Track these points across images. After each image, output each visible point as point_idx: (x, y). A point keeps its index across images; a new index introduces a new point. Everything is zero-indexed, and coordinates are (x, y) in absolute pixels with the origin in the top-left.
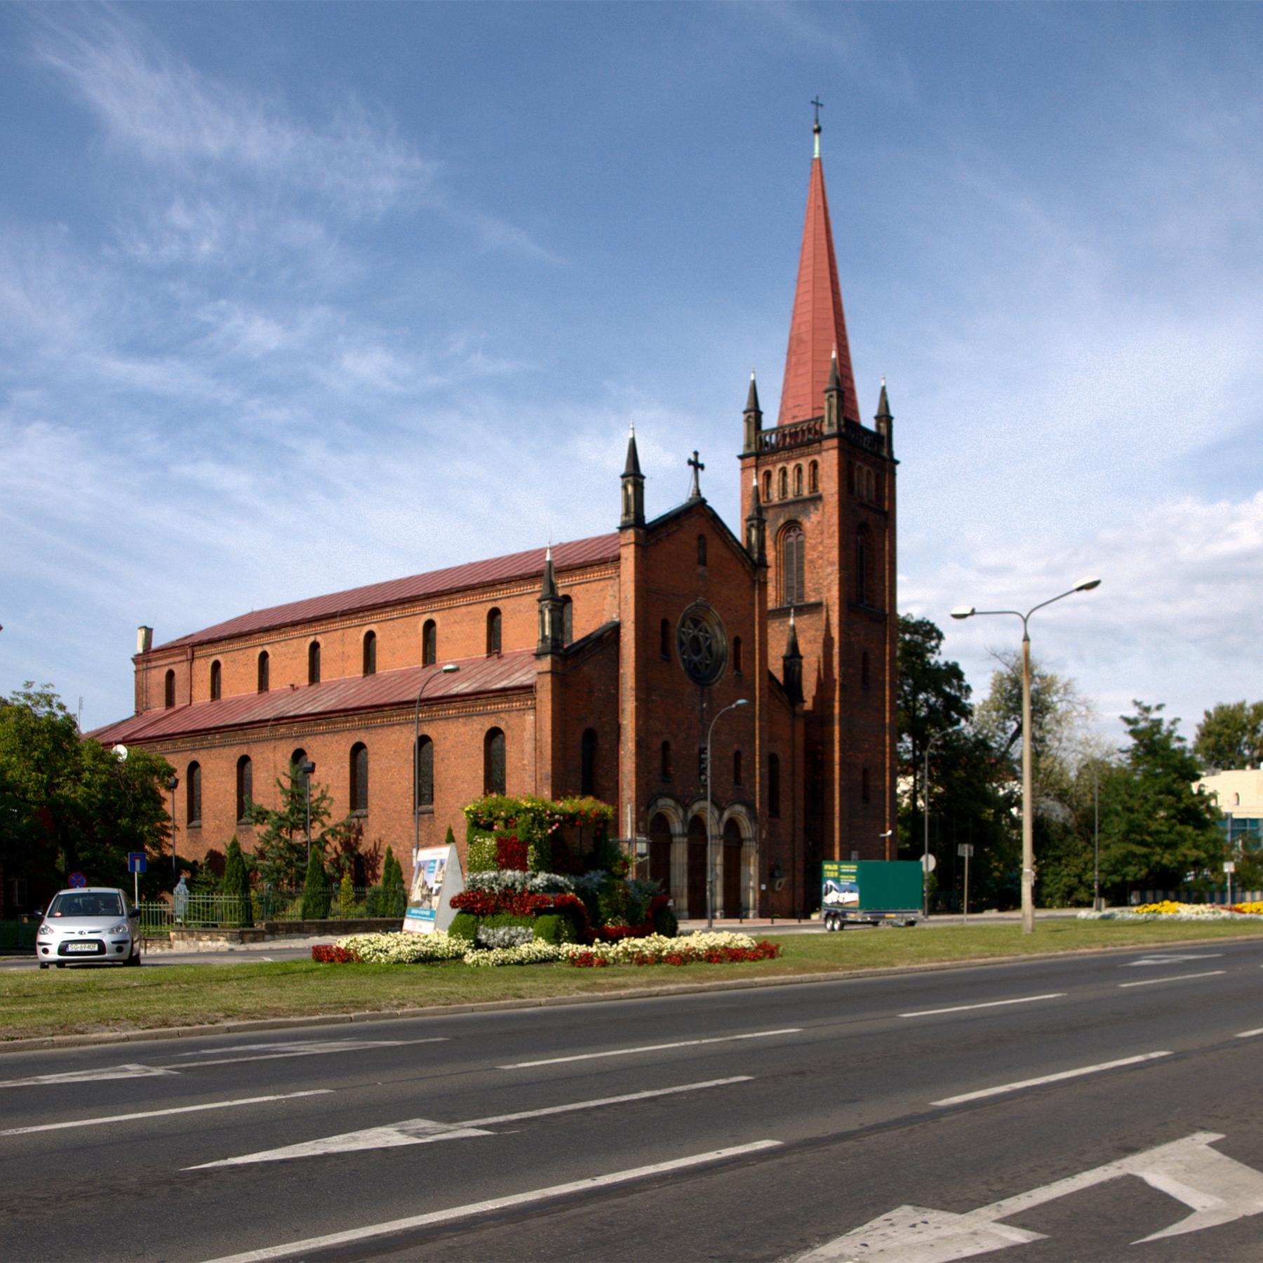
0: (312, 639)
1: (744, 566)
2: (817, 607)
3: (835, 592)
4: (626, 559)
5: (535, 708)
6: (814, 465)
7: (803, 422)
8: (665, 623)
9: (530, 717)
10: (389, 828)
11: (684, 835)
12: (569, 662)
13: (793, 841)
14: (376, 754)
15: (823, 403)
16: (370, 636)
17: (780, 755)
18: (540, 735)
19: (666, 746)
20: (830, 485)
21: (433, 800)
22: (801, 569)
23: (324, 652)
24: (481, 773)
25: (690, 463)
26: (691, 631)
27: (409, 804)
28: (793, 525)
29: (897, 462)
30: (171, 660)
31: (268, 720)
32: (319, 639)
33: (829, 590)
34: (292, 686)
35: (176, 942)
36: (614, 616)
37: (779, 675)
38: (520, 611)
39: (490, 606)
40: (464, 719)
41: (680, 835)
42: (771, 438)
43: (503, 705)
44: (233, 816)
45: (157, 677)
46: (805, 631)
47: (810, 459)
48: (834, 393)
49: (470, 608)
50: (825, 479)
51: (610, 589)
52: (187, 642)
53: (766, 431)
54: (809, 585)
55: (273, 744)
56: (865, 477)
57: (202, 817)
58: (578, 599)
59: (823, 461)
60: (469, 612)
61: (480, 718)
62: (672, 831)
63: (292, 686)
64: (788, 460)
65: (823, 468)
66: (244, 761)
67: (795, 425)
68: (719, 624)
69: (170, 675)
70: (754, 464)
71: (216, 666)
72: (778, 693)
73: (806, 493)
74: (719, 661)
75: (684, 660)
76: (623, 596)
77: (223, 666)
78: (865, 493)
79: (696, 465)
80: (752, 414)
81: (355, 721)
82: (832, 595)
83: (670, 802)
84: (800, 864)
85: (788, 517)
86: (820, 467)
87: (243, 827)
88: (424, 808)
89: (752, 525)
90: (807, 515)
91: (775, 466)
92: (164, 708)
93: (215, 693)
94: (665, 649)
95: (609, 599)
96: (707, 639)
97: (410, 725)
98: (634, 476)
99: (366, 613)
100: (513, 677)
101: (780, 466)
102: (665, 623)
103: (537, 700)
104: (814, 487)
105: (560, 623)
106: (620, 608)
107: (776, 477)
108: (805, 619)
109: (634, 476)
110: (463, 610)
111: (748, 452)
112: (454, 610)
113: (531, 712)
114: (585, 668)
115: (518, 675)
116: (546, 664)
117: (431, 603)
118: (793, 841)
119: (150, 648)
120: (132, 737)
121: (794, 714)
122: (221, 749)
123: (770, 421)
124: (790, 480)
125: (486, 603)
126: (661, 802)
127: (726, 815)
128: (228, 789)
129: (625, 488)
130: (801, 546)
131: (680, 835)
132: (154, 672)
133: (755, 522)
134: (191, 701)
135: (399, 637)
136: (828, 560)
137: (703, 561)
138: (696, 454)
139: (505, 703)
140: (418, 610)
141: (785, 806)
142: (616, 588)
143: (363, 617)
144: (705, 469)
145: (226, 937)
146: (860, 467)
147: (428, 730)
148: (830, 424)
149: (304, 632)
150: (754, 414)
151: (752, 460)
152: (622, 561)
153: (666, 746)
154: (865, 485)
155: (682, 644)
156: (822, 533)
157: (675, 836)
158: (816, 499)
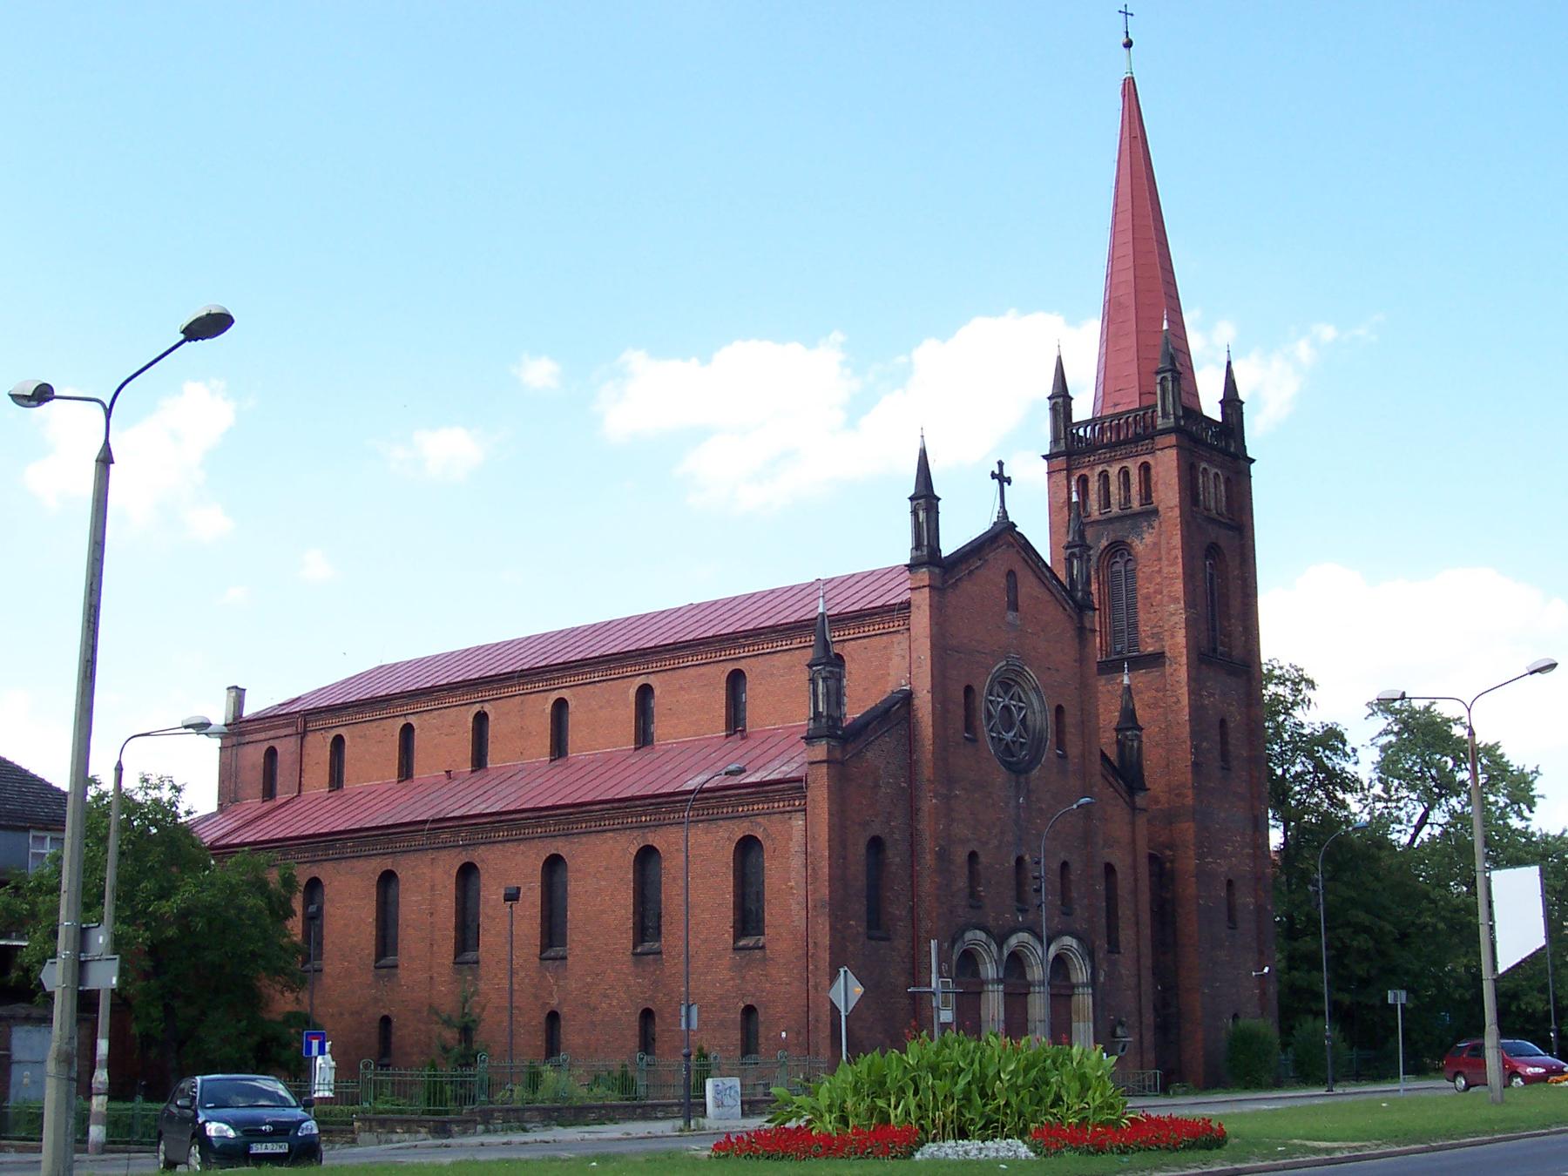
0: (477, 708)
1: (1065, 609)
2: (1157, 659)
3: (1181, 638)
4: (918, 608)
5: (805, 810)
6: (1146, 468)
7: (1129, 412)
8: (969, 690)
9: (798, 822)
10: (597, 975)
11: (999, 981)
12: (849, 748)
13: (1139, 985)
14: (579, 871)
15: (1155, 387)
16: (560, 705)
17: (1118, 867)
18: (812, 847)
19: (973, 856)
20: (1168, 494)
21: (660, 933)
22: (1132, 606)
23: (493, 728)
24: (730, 898)
25: (993, 476)
26: (1000, 700)
27: (627, 939)
28: (1119, 548)
29: (1220, 402)
30: (272, 733)
31: (424, 822)
32: (487, 708)
33: (1173, 636)
34: (448, 772)
35: (362, 1134)
36: (903, 682)
37: (1112, 754)
38: (772, 675)
39: (730, 667)
40: (706, 824)
41: (994, 982)
42: (1085, 431)
43: (761, 806)
44: (369, 955)
45: (254, 755)
46: (1142, 693)
47: (1141, 460)
48: (1168, 375)
49: (703, 669)
50: (1160, 487)
51: (899, 644)
52: (296, 708)
53: (1080, 424)
54: (1144, 629)
55: (431, 855)
56: (1212, 483)
57: (324, 956)
58: (853, 660)
59: (1157, 464)
60: (701, 675)
61: (727, 822)
62: (983, 975)
63: (448, 772)
64: (1109, 462)
65: (1157, 473)
66: (388, 879)
67: (1118, 416)
68: (1036, 690)
69: (271, 753)
70: (1065, 466)
71: (338, 742)
72: (1111, 779)
73: (1135, 505)
74: (1038, 743)
75: (993, 738)
76: (914, 656)
77: (347, 742)
78: (1213, 504)
79: (1001, 478)
80: (1060, 400)
81: (550, 825)
82: (1177, 643)
83: (981, 935)
84: (1149, 1018)
85: (1112, 537)
86: (1153, 472)
87: (384, 971)
88: (647, 946)
89: (1072, 554)
90: (1140, 535)
91: (1093, 469)
92: (260, 800)
93: (336, 781)
94: (969, 725)
95: (896, 660)
96: (1021, 708)
97: (628, 832)
98: (925, 500)
99: (556, 675)
100: (771, 766)
101: (1099, 469)
102: (969, 690)
103: (808, 799)
104: (1147, 496)
105: (836, 696)
106: (910, 674)
107: (1094, 485)
108: (1142, 675)
109: (925, 500)
110: (692, 671)
111: (1055, 451)
112: (680, 671)
113: (801, 815)
114: (869, 755)
115: (777, 763)
116: (820, 750)
117: (648, 662)
118: (1139, 985)
119: (241, 716)
120: (223, 842)
121: (1133, 808)
122: (355, 860)
123: (1082, 410)
124: (1113, 488)
125: (725, 664)
126: (969, 935)
127: (1053, 950)
128: (363, 916)
129: (915, 513)
130: (1131, 576)
131: (994, 982)
132: (249, 749)
133: (1076, 550)
134: (300, 792)
135: (601, 708)
136: (1170, 596)
137: (1014, 605)
138: (1001, 464)
139: (763, 803)
140: (629, 671)
141: (1126, 935)
142: (905, 645)
143: (551, 679)
144: (1012, 483)
145: (429, 1128)
146: (1205, 469)
147: (655, 839)
148: (1165, 415)
149: (466, 699)
150: (1061, 399)
151: (1061, 462)
152: (913, 608)
153: (973, 856)
154: (1213, 493)
155: (990, 716)
156: (1160, 559)
157: (986, 982)
158: (1150, 513)
